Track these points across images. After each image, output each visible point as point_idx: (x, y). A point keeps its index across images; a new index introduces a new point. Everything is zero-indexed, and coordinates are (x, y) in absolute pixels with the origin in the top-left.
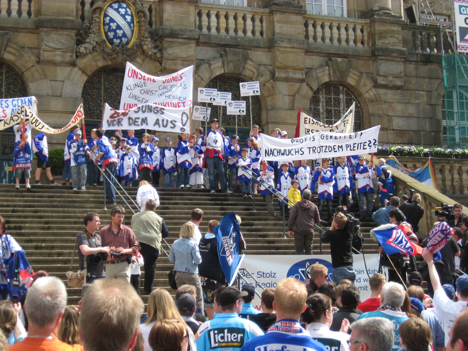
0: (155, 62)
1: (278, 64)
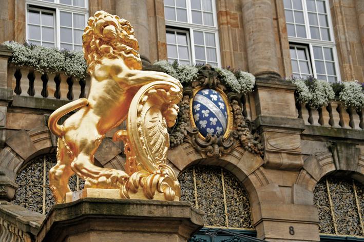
0: (255, 155)
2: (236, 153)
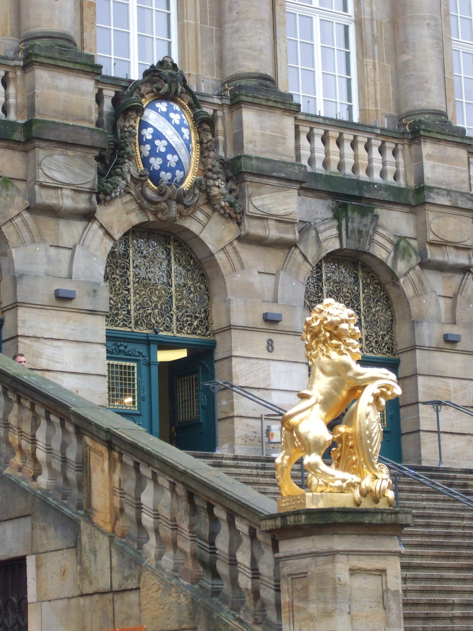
0: (229, 220)
1: (431, 237)
2: (199, 215)
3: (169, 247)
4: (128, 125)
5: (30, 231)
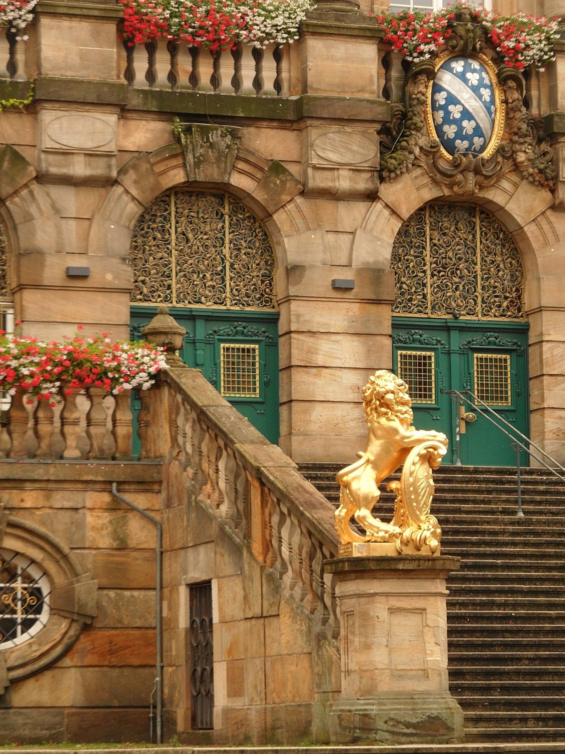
0: (540, 188)
3: (474, 220)
4: (416, 92)
5: (304, 218)
